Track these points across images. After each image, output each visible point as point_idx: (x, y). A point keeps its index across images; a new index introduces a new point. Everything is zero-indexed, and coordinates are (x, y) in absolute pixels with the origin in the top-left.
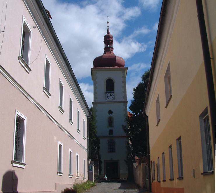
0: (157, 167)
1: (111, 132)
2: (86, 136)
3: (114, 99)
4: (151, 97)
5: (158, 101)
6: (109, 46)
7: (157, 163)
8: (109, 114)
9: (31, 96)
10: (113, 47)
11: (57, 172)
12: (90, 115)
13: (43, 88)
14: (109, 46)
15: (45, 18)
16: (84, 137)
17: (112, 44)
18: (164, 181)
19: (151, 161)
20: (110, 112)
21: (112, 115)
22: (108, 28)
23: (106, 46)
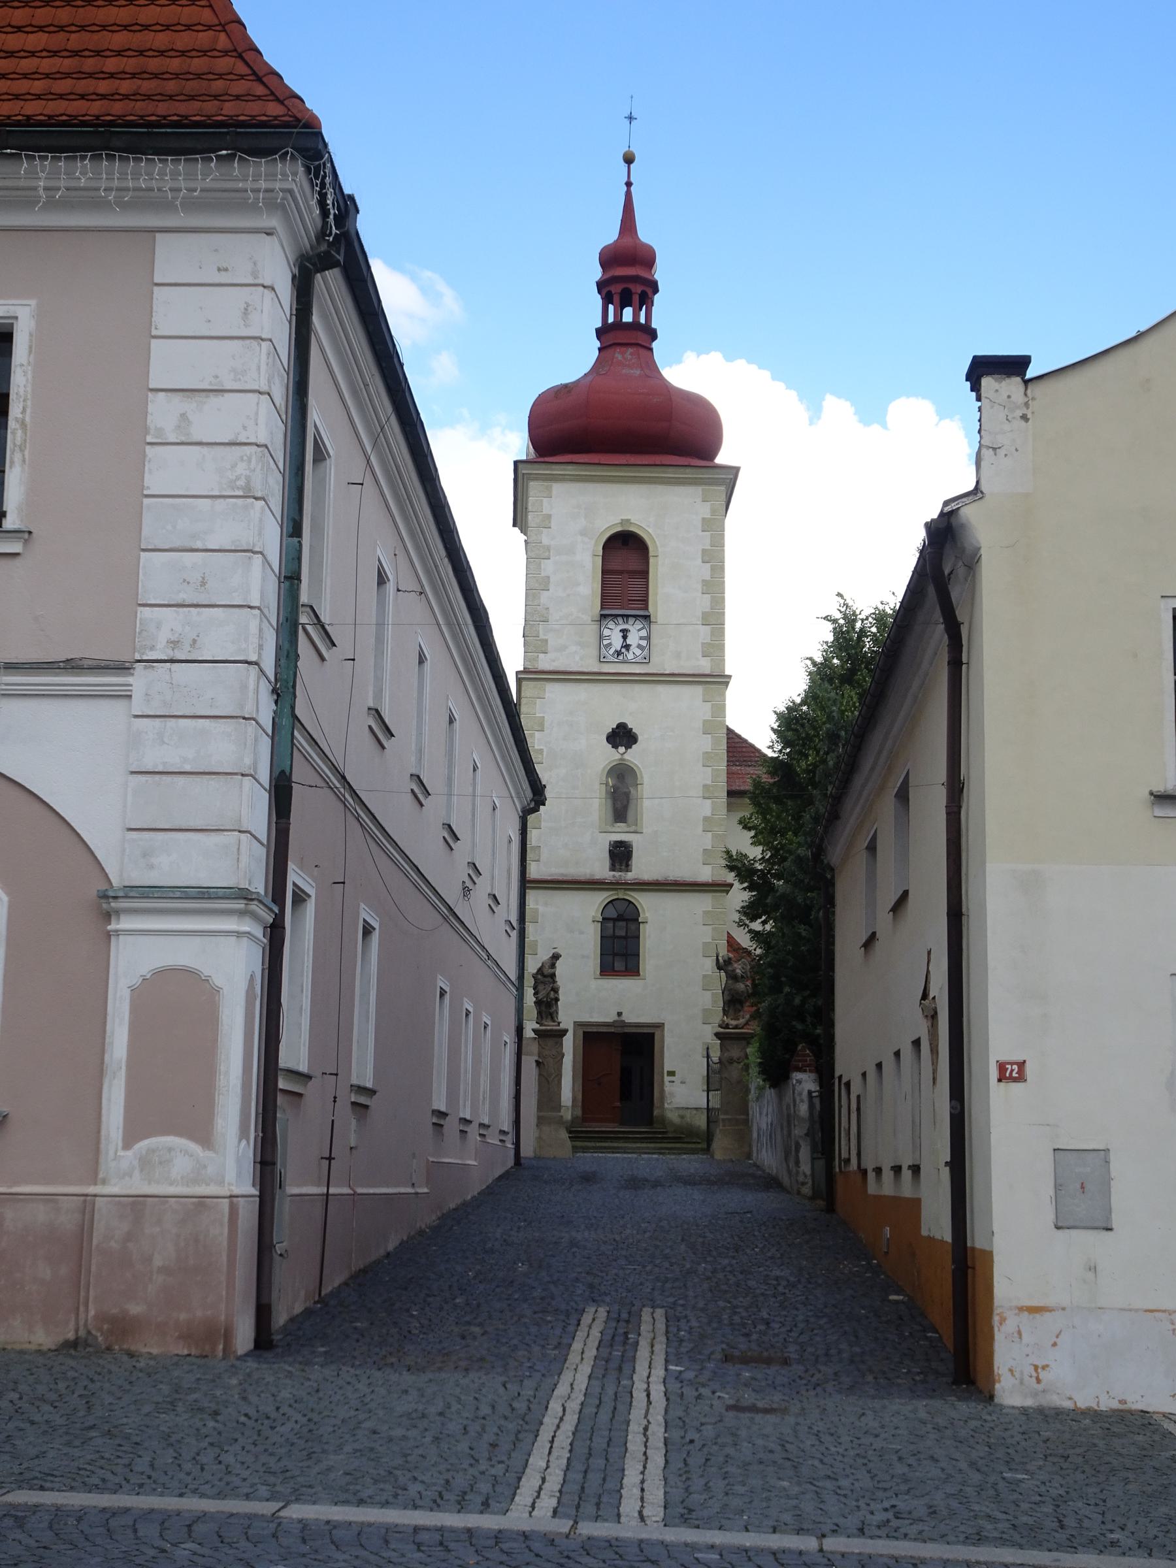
1: (621, 855)
6: (628, 315)
8: (615, 746)
14: (628, 315)
19: (840, 1077)
20: (622, 736)
21: (633, 756)
23: (611, 320)
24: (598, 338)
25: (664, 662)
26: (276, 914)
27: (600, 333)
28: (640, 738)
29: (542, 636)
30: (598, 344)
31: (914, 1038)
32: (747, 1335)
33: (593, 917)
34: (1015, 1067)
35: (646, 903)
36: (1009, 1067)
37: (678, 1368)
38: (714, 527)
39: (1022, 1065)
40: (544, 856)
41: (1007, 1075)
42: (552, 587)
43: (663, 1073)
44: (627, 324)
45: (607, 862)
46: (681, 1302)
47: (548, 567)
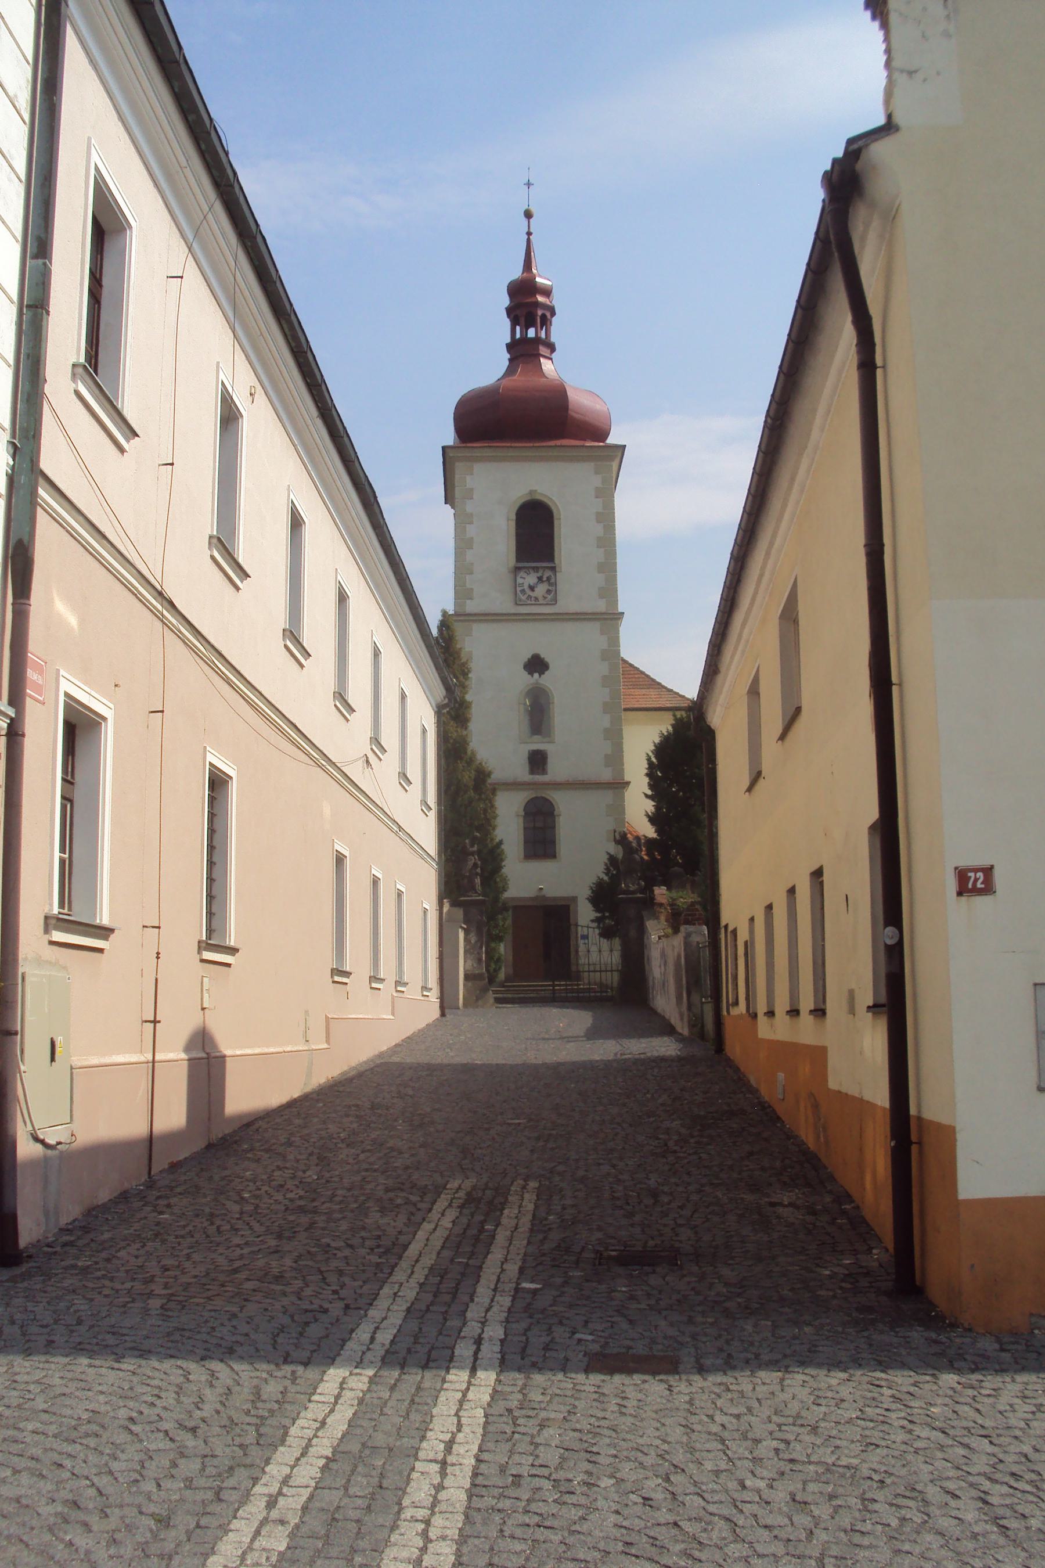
0: (746, 954)
1: (538, 761)
2: (432, 799)
3: (555, 601)
4: (731, 662)
5: (754, 691)
6: (531, 333)
7: (748, 938)
8: (531, 673)
9: (248, 679)
10: (553, 339)
11: (332, 970)
12: (450, 700)
13: (211, 537)
14: (531, 333)
15: (293, 344)
16: (424, 802)
17: (545, 322)
18: (771, 1014)
19: (726, 927)
20: (536, 665)
21: (546, 680)
22: (529, 241)
23: (518, 336)
24: (509, 351)
25: (567, 603)
26: (12, 719)
27: (510, 347)
28: (551, 666)
29: (468, 586)
30: (508, 356)
31: (813, 869)
32: (630, 1215)
34: (980, 875)
35: (561, 800)
36: (972, 874)
37: (533, 1286)
38: (606, 493)
39: (988, 871)
41: (970, 886)
44: (531, 338)
45: (527, 768)
46: (561, 1168)
47: (471, 531)
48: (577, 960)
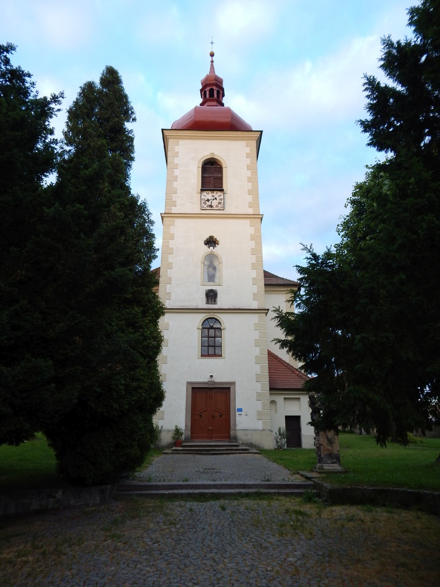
21: (217, 250)
22: (212, 66)
25: (229, 209)
28: (220, 242)
29: (173, 200)
33: (198, 327)
35: (223, 318)
40: (173, 296)
42: (178, 180)
43: (235, 410)
48: (235, 427)
